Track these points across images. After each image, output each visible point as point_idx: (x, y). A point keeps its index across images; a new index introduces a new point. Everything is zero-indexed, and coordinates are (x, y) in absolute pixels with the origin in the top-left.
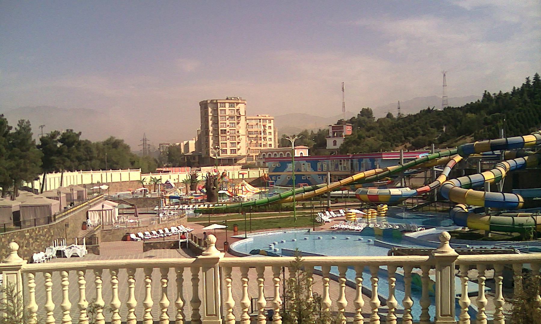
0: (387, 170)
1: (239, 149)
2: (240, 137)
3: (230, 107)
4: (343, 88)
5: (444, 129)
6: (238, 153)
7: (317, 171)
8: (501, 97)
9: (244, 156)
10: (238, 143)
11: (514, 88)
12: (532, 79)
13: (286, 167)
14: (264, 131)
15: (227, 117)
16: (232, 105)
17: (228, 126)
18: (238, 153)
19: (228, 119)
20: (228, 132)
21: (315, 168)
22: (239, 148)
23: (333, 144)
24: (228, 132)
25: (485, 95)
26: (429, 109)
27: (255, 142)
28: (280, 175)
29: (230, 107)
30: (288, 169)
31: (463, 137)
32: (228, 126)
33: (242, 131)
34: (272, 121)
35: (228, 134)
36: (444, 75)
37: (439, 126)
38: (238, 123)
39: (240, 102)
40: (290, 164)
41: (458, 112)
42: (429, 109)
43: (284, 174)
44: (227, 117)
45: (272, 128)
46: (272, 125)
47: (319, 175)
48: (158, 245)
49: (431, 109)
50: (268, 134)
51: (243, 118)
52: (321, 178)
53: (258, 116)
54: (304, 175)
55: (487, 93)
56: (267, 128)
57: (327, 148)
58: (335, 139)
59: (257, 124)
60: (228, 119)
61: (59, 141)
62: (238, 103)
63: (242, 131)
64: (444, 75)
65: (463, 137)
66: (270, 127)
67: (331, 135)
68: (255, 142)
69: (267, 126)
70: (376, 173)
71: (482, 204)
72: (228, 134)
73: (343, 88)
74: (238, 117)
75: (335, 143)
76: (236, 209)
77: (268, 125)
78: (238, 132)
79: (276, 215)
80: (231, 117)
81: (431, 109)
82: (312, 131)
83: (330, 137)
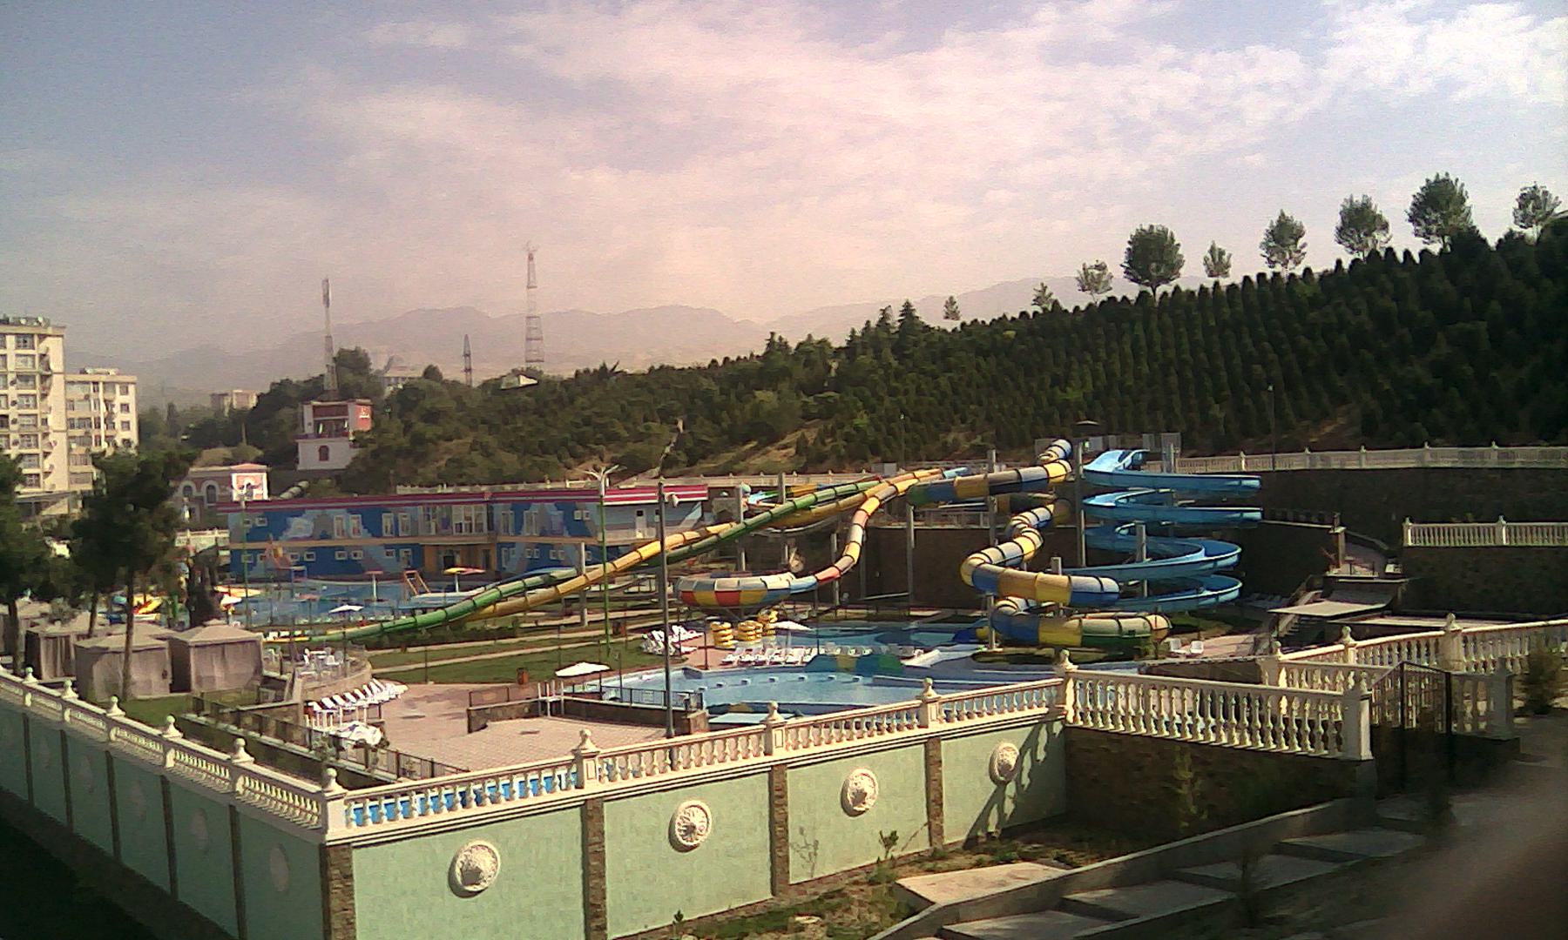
0: (709, 535)
1: (47, 474)
2: (51, 438)
3: (18, 347)
4: (326, 297)
5: (680, 425)
6: (47, 484)
7: (380, 536)
8: (813, 351)
9: (63, 495)
10: (46, 455)
11: (853, 331)
12: (895, 317)
13: (286, 527)
14: (109, 420)
15: (11, 377)
16: (24, 340)
17: (14, 403)
18: (47, 484)
19: (13, 383)
20: (14, 422)
21: (374, 529)
22: (47, 468)
23: (317, 455)
24: (14, 422)
25: (771, 343)
26: (604, 367)
27: (82, 450)
28: (263, 550)
29: (18, 347)
30: (290, 534)
31: (756, 449)
32: (14, 403)
33: (56, 421)
34: (131, 388)
35: (13, 427)
36: (531, 258)
37: (667, 417)
38: (44, 396)
39: (50, 331)
40: (297, 520)
41: (706, 383)
42: (604, 367)
43: (279, 550)
44: (11, 377)
45: (132, 407)
46: (130, 399)
47: (387, 546)
48: (500, 713)
49: (610, 367)
50: (118, 426)
51: (57, 382)
52: (393, 557)
53: (84, 372)
54: (341, 548)
55: (776, 339)
56: (116, 410)
57: (300, 468)
58: (324, 442)
59: (87, 398)
60: (13, 383)
61: (1396, 552)
62: (42, 337)
63: (56, 421)
64: (531, 258)
65: (756, 449)
66: (125, 407)
67: (309, 430)
68: (82, 450)
69: (117, 403)
70: (687, 542)
71: (1067, 598)
72: (13, 427)
73: (326, 297)
74: (44, 378)
75: (324, 453)
76: (374, 639)
77: (119, 399)
78: (45, 421)
79: (508, 647)
80: (24, 378)
81: (610, 367)
82: (171, 406)
83: (306, 437)
